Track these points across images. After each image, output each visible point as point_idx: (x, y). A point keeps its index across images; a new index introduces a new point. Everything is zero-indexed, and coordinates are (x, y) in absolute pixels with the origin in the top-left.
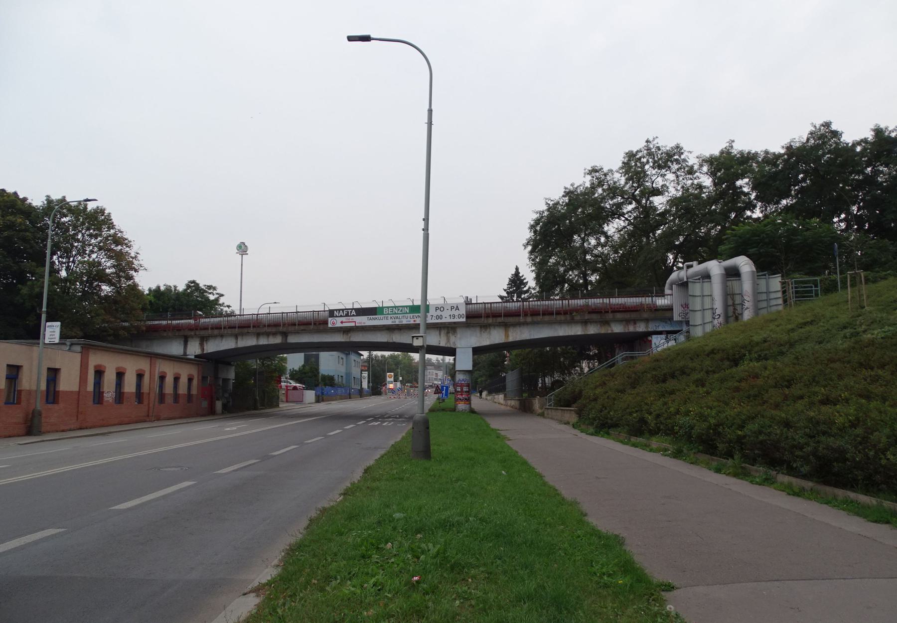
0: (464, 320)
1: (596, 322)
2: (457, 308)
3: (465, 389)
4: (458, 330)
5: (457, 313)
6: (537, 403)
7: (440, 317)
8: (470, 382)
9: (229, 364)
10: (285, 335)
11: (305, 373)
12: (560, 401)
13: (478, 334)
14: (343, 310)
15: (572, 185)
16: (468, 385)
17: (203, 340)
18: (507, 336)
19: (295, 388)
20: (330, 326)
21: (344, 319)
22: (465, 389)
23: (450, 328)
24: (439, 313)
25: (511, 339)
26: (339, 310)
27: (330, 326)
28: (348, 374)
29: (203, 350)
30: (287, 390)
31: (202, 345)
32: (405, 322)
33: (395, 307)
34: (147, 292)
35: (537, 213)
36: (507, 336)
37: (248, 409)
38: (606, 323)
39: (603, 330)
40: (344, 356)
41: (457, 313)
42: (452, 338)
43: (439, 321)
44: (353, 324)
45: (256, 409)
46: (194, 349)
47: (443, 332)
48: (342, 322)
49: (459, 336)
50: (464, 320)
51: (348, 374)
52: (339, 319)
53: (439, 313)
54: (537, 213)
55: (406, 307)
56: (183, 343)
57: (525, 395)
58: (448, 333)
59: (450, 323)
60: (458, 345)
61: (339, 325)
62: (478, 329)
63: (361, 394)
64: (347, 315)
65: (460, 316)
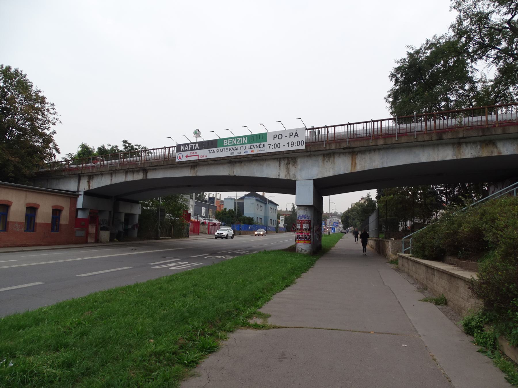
0: (303, 147)
1: (474, 142)
2: (297, 135)
3: (305, 226)
4: (299, 161)
5: (295, 140)
6: (390, 245)
7: (277, 146)
8: (312, 219)
9: (137, 202)
10: (145, 171)
11: (225, 214)
12: (423, 248)
13: (321, 163)
14: (188, 144)
15: (434, 37)
16: (309, 222)
17: (91, 177)
18: (354, 165)
19: (215, 224)
20: (177, 160)
21: (189, 153)
22: (305, 226)
23: (289, 158)
24: (277, 141)
25: (359, 168)
26: (185, 144)
27: (177, 160)
28: (266, 217)
29: (89, 186)
30: (209, 225)
31: (89, 182)
32: (243, 153)
33: (235, 138)
34: (96, 150)
35: (398, 62)
36: (354, 165)
37: (149, 238)
38: (491, 142)
39: (485, 153)
40: (263, 205)
41: (295, 140)
42: (292, 170)
43: (277, 150)
44: (196, 158)
45: (157, 238)
46: (84, 186)
47: (283, 163)
48: (187, 157)
49: (299, 167)
50: (303, 147)
51: (266, 217)
52: (185, 154)
53: (277, 141)
54: (398, 62)
55: (245, 137)
56: (77, 181)
57: (382, 236)
58: (288, 164)
59: (288, 152)
60: (298, 177)
61: (184, 159)
62: (320, 159)
63: (277, 230)
64: (192, 149)
65: (299, 143)
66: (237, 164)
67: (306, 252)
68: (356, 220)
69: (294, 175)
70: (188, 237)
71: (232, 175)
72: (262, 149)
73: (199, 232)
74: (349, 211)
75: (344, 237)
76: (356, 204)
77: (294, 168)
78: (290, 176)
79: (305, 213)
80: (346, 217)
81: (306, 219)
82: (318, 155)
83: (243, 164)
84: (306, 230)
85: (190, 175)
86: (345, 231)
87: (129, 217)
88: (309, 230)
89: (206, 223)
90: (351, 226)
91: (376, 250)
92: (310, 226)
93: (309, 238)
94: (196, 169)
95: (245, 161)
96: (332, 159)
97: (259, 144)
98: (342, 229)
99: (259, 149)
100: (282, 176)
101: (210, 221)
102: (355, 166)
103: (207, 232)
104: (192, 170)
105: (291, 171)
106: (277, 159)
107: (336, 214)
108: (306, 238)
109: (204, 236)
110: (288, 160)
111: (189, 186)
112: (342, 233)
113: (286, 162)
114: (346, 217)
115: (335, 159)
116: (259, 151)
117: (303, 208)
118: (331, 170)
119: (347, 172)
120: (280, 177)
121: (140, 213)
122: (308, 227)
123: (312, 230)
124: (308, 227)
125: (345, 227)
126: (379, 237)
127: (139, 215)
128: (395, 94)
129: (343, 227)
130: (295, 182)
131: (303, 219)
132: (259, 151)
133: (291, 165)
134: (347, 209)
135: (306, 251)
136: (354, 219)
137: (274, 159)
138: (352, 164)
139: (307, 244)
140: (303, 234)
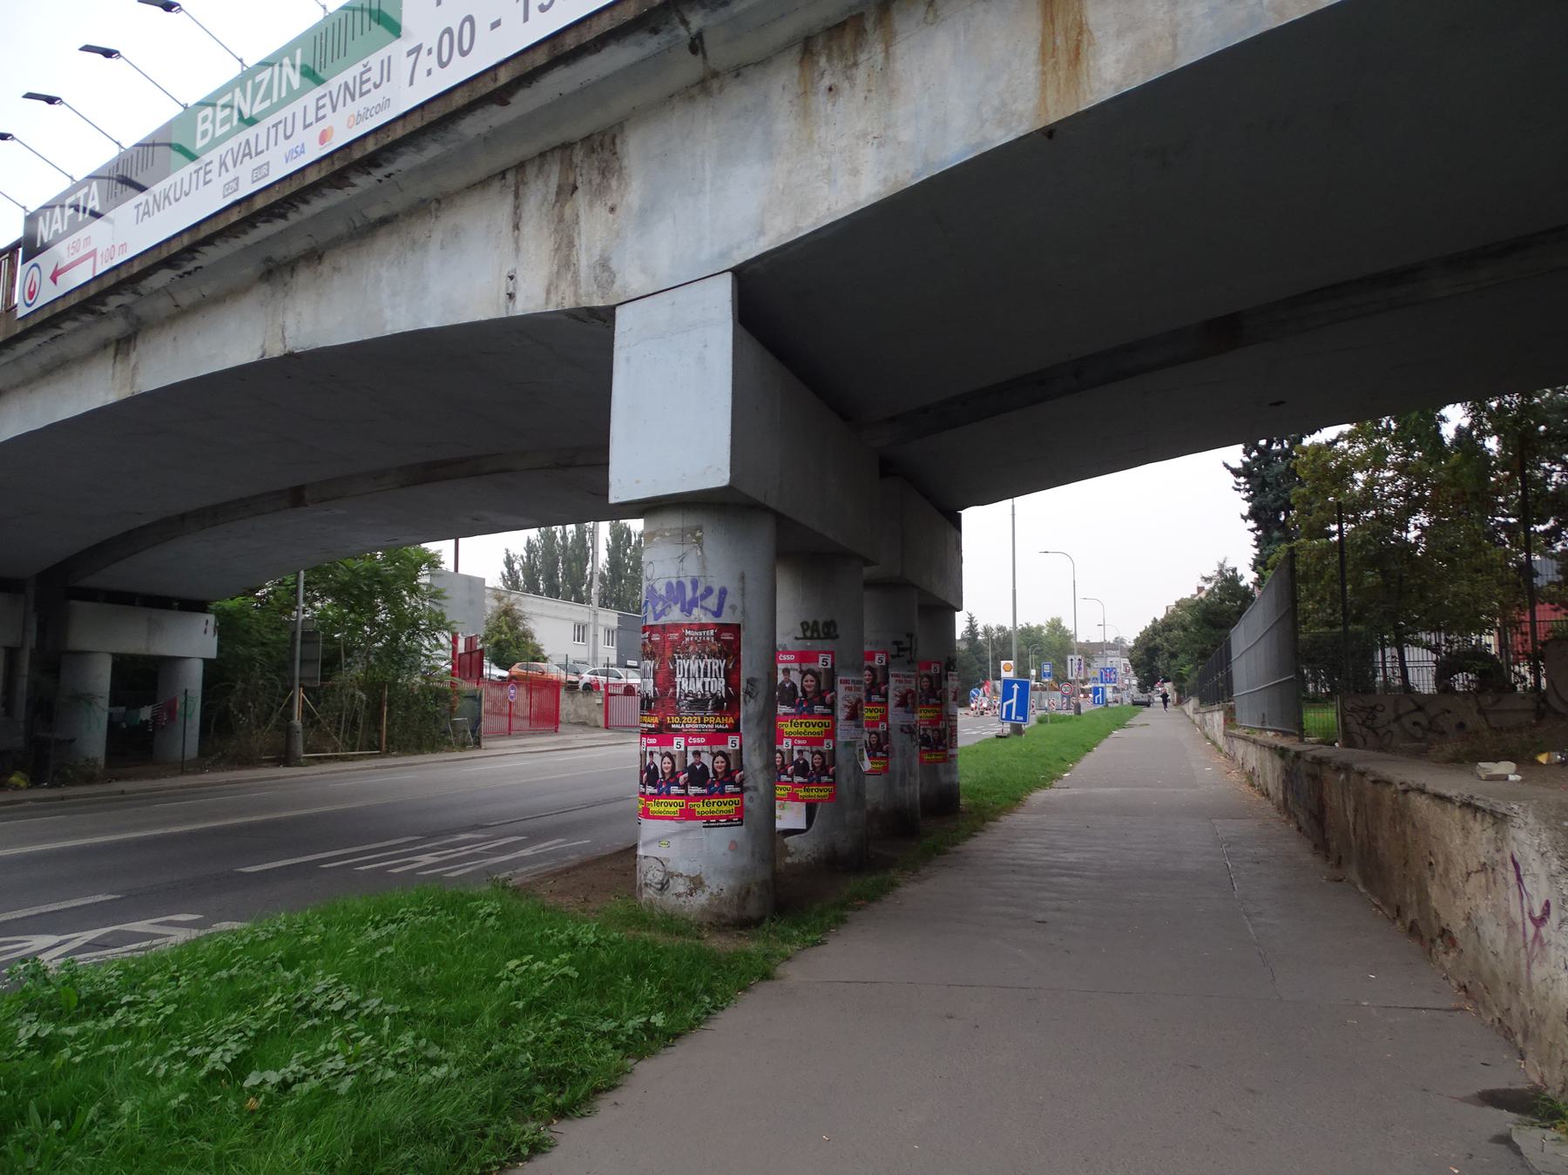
9: (200, 606)
13: (785, 125)
42: (594, 227)
47: (539, 192)
58: (567, 191)
60: (632, 279)
62: (782, 82)
66: (303, 276)
67: (701, 899)
68: (1182, 658)
69: (604, 264)
70: (478, 744)
71: (276, 351)
72: (374, 98)
73: (557, 722)
74: (1158, 630)
75: (1135, 721)
76: (1178, 604)
77: (601, 211)
78: (576, 282)
79: (692, 568)
80: (1148, 650)
81: (698, 616)
82: (763, 62)
83: (325, 268)
84: (698, 703)
85: (112, 398)
86: (1143, 698)
87: (142, 678)
88: (727, 704)
89: (598, 686)
90: (1167, 680)
91: (1284, 807)
92: (731, 676)
93: (728, 777)
94: (133, 356)
95: (337, 242)
96: (872, 54)
97: (357, 69)
98: (1134, 691)
99: (361, 104)
100: (532, 299)
101: (612, 680)
102: (1076, 55)
103: (601, 722)
104: (119, 367)
105: (582, 242)
106: (503, 174)
107: (1117, 645)
108: (698, 775)
109: (580, 737)
110: (568, 165)
111: (296, 497)
112: (1135, 704)
113: (554, 180)
114: (1148, 650)
115: (900, 49)
116: (361, 117)
117: (672, 522)
118: (868, 156)
119: (1000, 137)
120: (521, 308)
121: (212, 653)
122: (718, 686)
123: (748, 709)
124: (718, 686)
125: (1146, 684)
126: (1300, 732)
127: (206, 661)
128: (1253, 515)
129: (1140, 685)
130: (603, 318)
131: (675, 615)
132: (361, 117)
133: (581, 198)
134: (1149, 624)
135: (697, 883)
136: (1173, 656)
137: (484, 183)
138: (1047, 52)
139: (711, 821)
140: (678, 744)
